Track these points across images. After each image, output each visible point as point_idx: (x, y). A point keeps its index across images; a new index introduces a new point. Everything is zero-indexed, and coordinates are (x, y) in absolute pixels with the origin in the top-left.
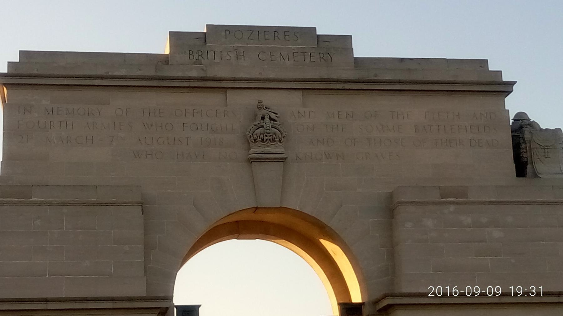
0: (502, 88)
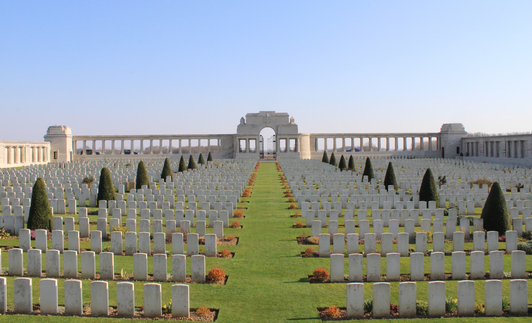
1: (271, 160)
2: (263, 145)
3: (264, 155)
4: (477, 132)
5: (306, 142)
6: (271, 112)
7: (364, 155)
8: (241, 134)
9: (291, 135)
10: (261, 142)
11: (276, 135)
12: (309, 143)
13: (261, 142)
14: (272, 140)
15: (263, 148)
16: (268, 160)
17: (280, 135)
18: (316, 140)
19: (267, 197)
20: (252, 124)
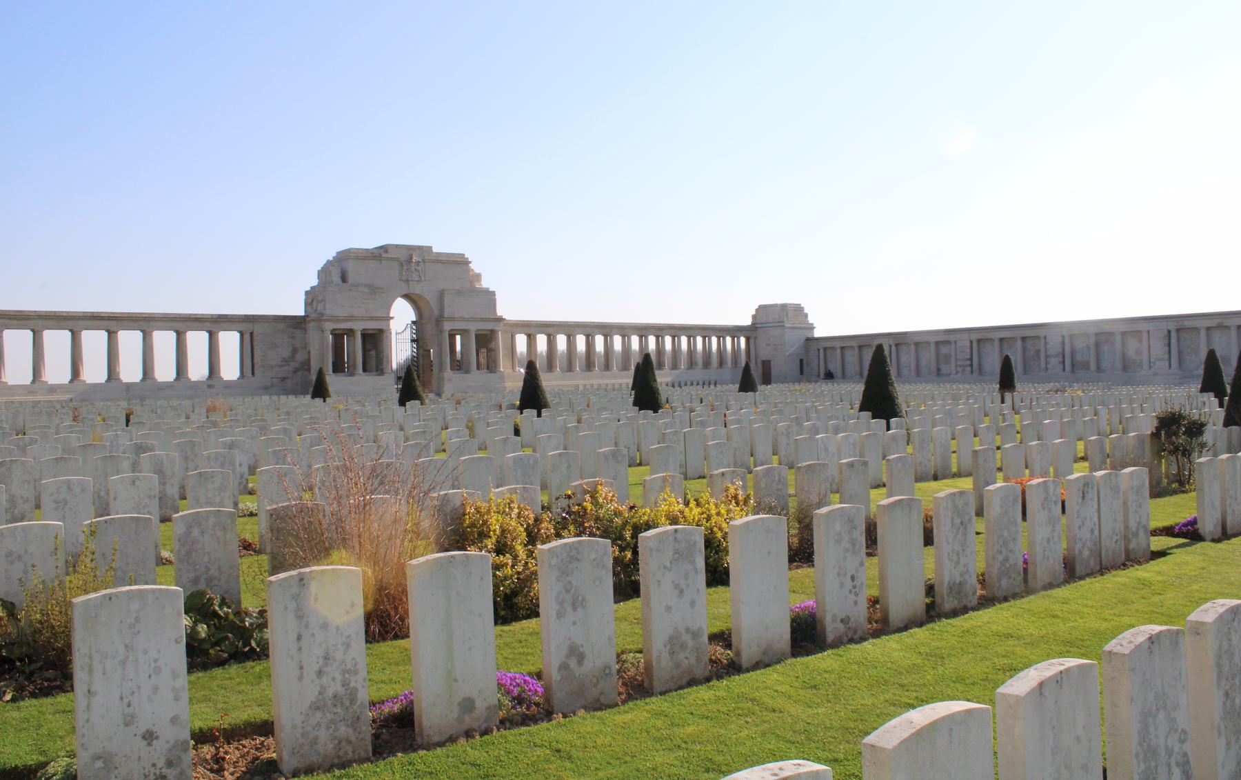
17: (453, 319)
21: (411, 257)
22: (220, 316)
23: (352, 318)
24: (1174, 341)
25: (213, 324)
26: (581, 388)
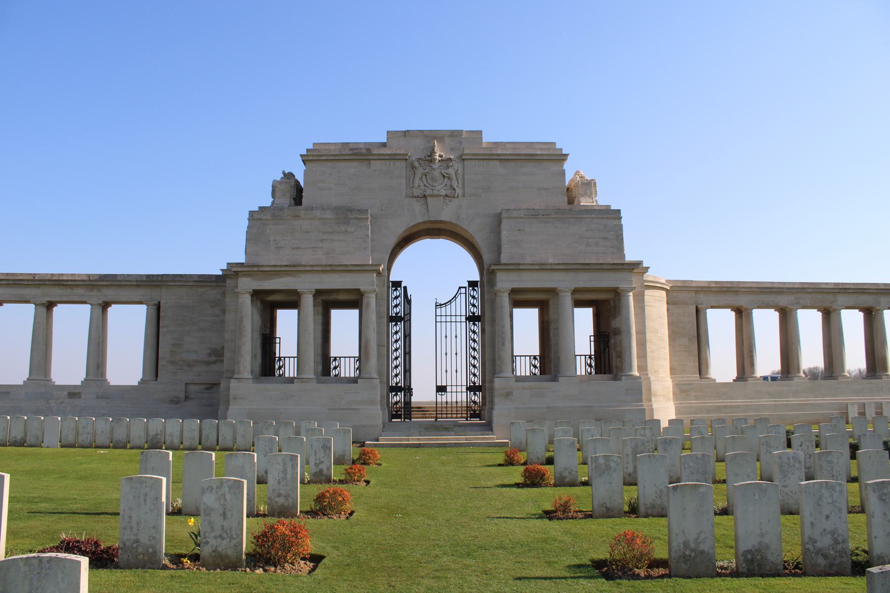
0: (562, 158)
1: (454, 428)
2: (407, 336)
3: (416, 398)
4: (812, 367)
5: (652, 325)
6: (455, 134)
7: (863, 399)
8: (269, 259)
9: (586, 268)
10: (396, 319)
11: (485, 284)
12: (665, 331)
13: (396, 319)
14: (460, 308)
15: (407, 371)
16: (437, 428)
17: (516, 268)
18: (699, 314)
19: (322, 240)
20: (343, 212)
21: (433, 152)
22: (104, 278)
23: (293, 269)
24: (256, 269)
25: (102, 291)
26: (853, 413)
